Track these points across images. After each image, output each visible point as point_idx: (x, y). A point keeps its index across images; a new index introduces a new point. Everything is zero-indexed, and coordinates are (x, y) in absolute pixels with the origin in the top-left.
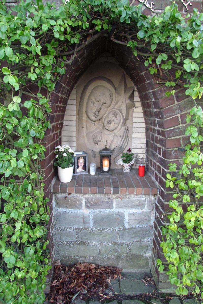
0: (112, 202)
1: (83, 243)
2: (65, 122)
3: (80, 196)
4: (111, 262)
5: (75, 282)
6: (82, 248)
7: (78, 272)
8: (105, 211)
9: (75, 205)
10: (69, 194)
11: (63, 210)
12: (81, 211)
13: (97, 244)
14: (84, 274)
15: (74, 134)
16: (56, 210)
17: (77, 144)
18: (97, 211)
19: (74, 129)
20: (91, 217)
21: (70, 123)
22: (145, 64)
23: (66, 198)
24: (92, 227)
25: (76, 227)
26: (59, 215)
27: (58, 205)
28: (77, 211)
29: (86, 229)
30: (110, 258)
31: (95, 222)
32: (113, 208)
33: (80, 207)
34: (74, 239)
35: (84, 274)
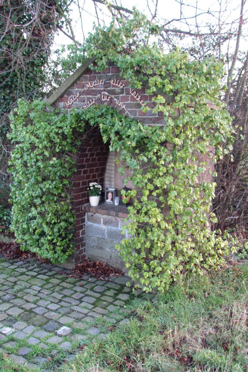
0: (118, 223)
1: (101, 248)
2: (107, 167)
3: (100, 215)
4: (118, 265)
5: (80, 263)
6: (100, 251)
7: (95, 263)
8: (114, 228)
9: (97, 221)
10: (94, 214)
11: (91, 223)
12: (100, 226)
13: (109, 250)
14: (98, 267)
15: (113, 176)
16: (87, 223)
17: (115, 183)
18: (110, 227)
19: (113, 172)
20: (106, 231)
21: (111, 168)
22: (162, 97)
23: (92, 215)
24: (106, 237)
25: (98, 236)
26: (89, 226)
27: (88, 220)
28: (98, 225)
29: (103, 238)
30: (117, 263)
31: (108, 235)
32: (118, 227)
33: (99, 223)
34: (96, 244)
35: (98, 267)
